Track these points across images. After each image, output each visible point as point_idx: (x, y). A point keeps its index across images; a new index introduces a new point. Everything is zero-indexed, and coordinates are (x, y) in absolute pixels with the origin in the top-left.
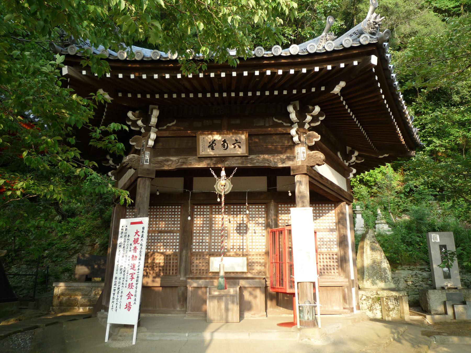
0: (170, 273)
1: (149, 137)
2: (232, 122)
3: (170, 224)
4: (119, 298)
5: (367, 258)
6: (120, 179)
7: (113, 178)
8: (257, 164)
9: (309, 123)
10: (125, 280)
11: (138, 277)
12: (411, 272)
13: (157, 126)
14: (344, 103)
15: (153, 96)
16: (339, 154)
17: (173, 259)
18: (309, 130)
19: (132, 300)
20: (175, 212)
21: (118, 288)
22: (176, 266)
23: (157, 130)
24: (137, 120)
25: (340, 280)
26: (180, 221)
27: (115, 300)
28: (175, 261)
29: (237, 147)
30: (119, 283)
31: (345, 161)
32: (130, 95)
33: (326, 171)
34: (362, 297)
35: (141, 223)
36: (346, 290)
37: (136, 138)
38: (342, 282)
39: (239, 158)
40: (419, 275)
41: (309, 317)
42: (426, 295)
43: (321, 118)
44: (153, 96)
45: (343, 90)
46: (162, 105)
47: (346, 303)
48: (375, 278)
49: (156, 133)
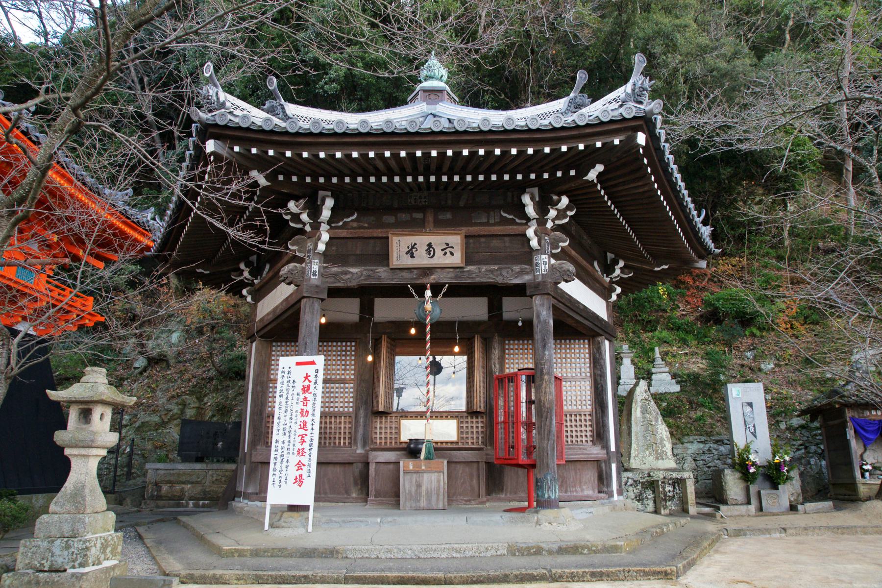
0: (340, 443)
1: (319, 239)
2: (441, 217)
4: (284, 469)
6: (259, 301)
7: (249, 299)
8: (477, 280)
10: (291, 445)
11: (312, 440)
12: (702, 446)
13: (329, 222)
14: (602, 193)
15: (328, 180)
16: (596, 264)
17: (345, 423)
18: (553, 229)
19: (304, 472)
20: (346, 351)
21: (282, 456)
22: (350, 433)
27: (277, 472)
28: (347, 426)
29: (448, 254)
30: (283, 448)
32: (294, 179)
33: (577, 290)
35: (313, 363)
36: (603, 465)
37: (298, 239)
40: (714, 451)
42: (721, 478)
43: (570, 213)
44: (328, 180)
45: (599, 176)
46: (337, 193)
48: (647, 452)
49: (328, 231)
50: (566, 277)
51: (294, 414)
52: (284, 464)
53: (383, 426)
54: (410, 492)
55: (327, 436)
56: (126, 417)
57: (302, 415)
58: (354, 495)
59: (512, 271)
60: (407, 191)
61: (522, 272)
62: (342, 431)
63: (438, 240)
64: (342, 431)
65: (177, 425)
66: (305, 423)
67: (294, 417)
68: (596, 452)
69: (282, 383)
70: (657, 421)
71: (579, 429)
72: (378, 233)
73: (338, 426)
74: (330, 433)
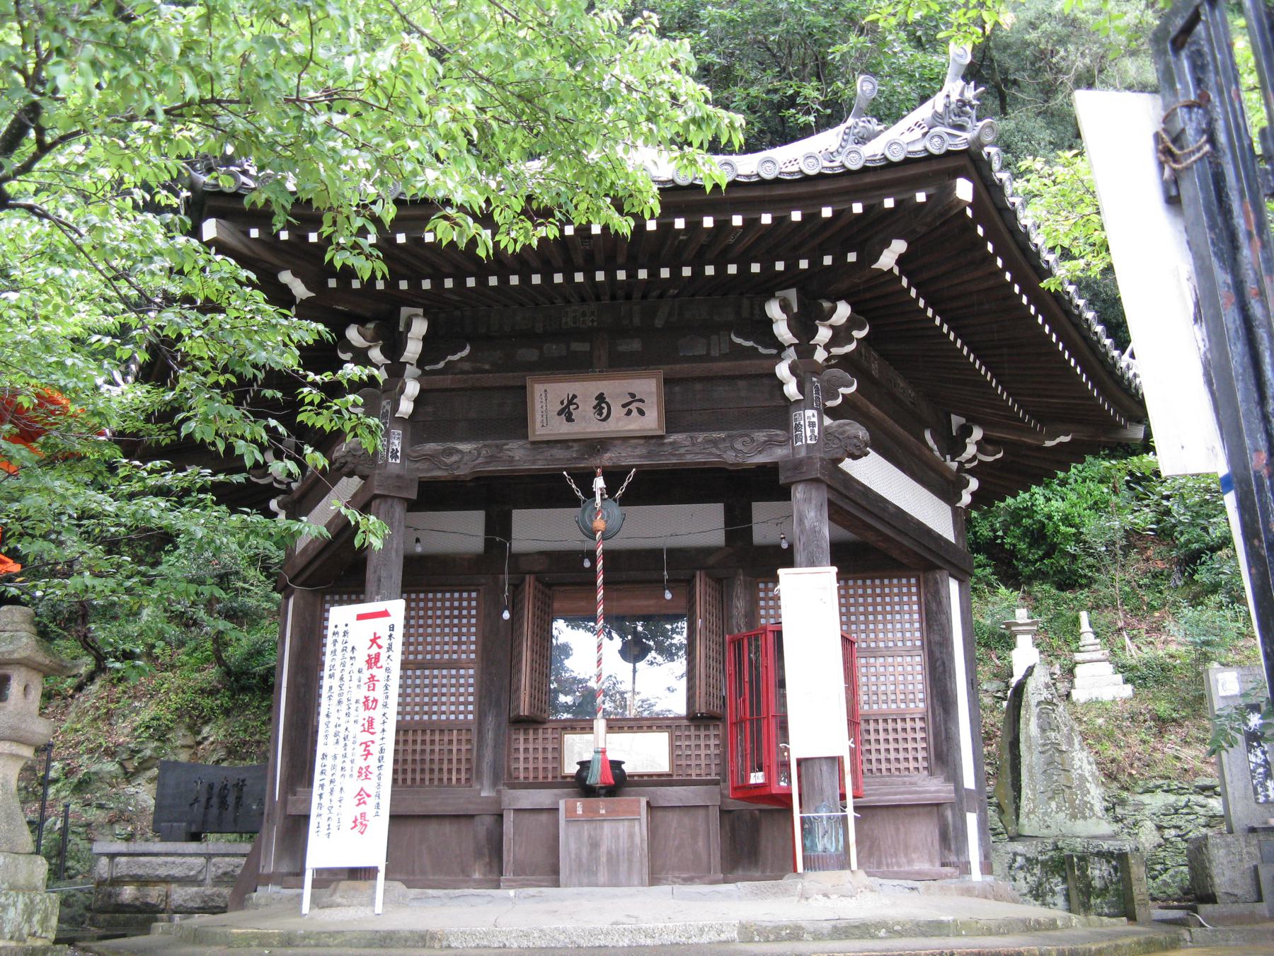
0: (450, 780)
3: (446, 643)
5: (1029, 748)
8: (689, 458)
9: (827, 347)
10: (348, 760)
11: (382, 750)
13: (421, 362)
14: (913, 293)
16: (928, 435)
17: (459, 741)
22: (468, 760)
23: (419, 372)
24: (370, 347)
25: (933, 789)
26: (475, 634)
27: (324, 811)
28: (464, 747)
29: (635, 412)
30: (334, 767)
31: (948, 457)
33: (875, 473)
34: (1014, 861)
35: (385, 614)
36: (949, 814)
38: (936, 792)
39: (642, 441)
41: (828, 846)
43: (859, 334)
45: (901, 260)
46: (433, 306)
47: (950, 850)
48: (1053, 804)
49: (418, 379)
50: (851, 449)
51: (353, 706)
52: (337, 794)
53: (531, 746)
54: (579, 857)
55: (427, 766)
56: (57, 765)
57: (367, 708)
58: (477, 876)
59: (753, 440)
60: (559, 302)
61: (770, 443)
62: (455, 758)
63: (615, 388)
64: (455, 758)
65: (151, 780)
66: (371, 722)
67: (352, 711)
68: (934, 788)
69: (334, 652)
70: (1070, 743)
71: (901, 745)
72: (508, 379)
73: (446, 747)
74: (432, 761)
